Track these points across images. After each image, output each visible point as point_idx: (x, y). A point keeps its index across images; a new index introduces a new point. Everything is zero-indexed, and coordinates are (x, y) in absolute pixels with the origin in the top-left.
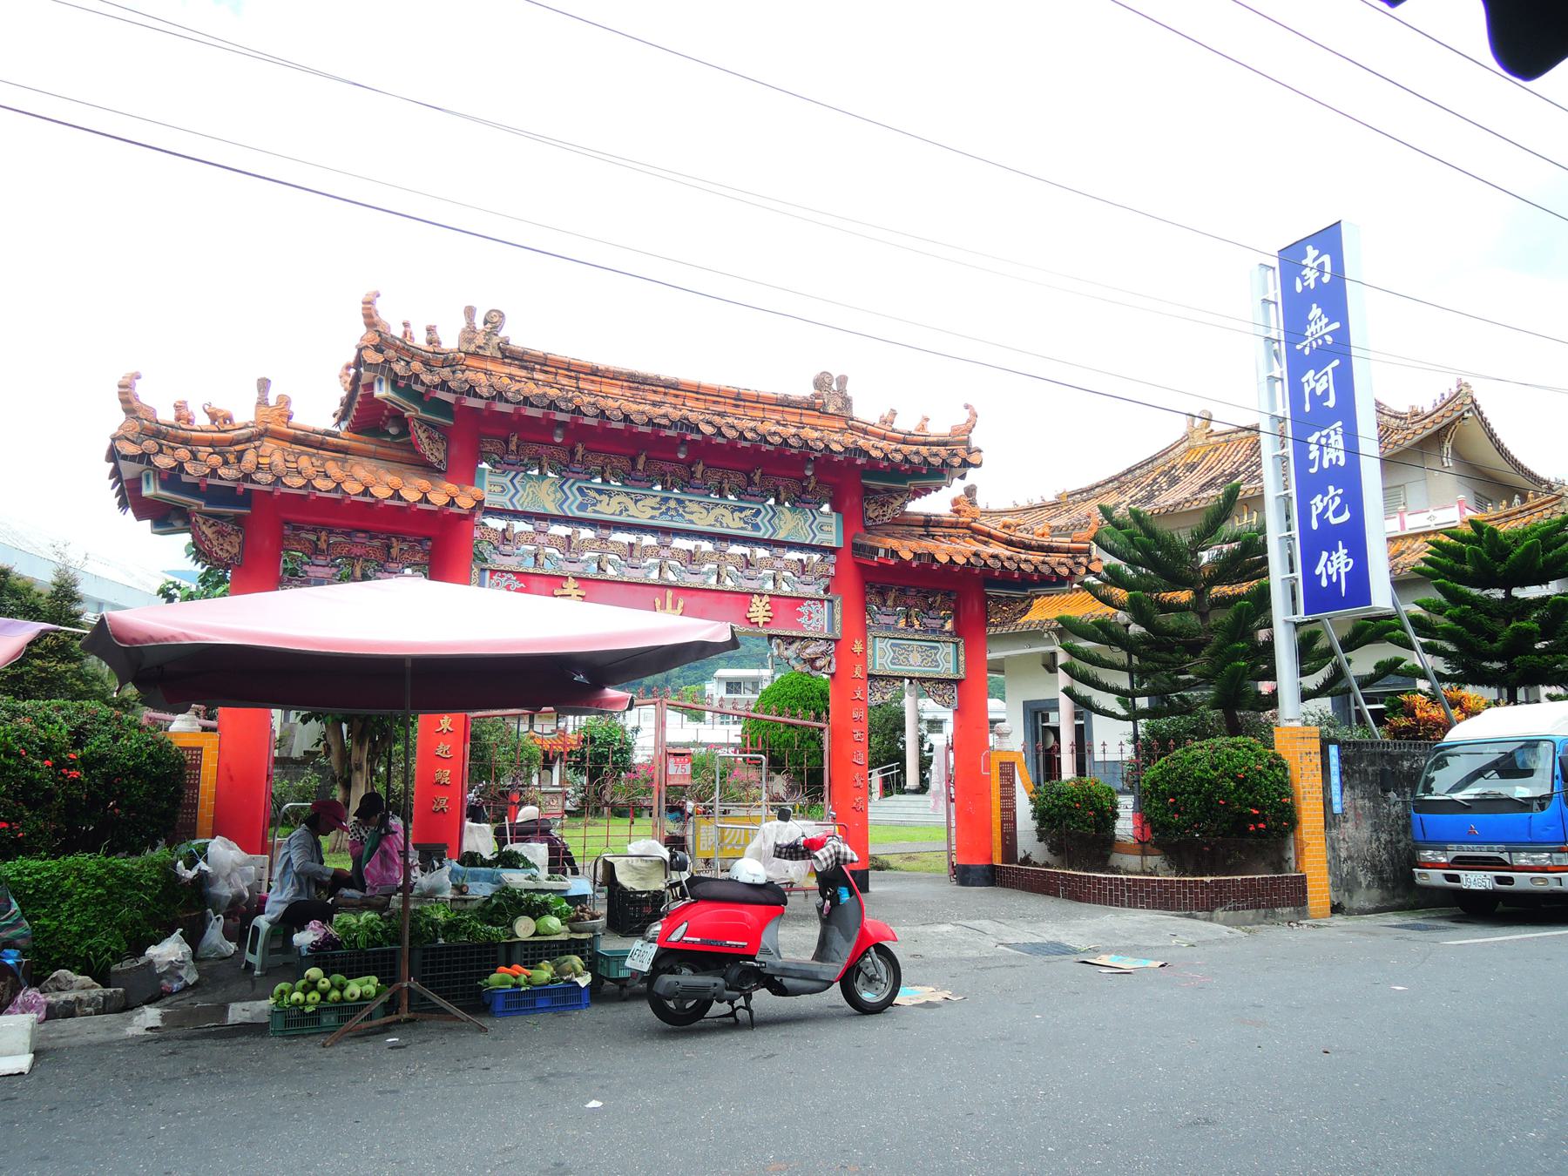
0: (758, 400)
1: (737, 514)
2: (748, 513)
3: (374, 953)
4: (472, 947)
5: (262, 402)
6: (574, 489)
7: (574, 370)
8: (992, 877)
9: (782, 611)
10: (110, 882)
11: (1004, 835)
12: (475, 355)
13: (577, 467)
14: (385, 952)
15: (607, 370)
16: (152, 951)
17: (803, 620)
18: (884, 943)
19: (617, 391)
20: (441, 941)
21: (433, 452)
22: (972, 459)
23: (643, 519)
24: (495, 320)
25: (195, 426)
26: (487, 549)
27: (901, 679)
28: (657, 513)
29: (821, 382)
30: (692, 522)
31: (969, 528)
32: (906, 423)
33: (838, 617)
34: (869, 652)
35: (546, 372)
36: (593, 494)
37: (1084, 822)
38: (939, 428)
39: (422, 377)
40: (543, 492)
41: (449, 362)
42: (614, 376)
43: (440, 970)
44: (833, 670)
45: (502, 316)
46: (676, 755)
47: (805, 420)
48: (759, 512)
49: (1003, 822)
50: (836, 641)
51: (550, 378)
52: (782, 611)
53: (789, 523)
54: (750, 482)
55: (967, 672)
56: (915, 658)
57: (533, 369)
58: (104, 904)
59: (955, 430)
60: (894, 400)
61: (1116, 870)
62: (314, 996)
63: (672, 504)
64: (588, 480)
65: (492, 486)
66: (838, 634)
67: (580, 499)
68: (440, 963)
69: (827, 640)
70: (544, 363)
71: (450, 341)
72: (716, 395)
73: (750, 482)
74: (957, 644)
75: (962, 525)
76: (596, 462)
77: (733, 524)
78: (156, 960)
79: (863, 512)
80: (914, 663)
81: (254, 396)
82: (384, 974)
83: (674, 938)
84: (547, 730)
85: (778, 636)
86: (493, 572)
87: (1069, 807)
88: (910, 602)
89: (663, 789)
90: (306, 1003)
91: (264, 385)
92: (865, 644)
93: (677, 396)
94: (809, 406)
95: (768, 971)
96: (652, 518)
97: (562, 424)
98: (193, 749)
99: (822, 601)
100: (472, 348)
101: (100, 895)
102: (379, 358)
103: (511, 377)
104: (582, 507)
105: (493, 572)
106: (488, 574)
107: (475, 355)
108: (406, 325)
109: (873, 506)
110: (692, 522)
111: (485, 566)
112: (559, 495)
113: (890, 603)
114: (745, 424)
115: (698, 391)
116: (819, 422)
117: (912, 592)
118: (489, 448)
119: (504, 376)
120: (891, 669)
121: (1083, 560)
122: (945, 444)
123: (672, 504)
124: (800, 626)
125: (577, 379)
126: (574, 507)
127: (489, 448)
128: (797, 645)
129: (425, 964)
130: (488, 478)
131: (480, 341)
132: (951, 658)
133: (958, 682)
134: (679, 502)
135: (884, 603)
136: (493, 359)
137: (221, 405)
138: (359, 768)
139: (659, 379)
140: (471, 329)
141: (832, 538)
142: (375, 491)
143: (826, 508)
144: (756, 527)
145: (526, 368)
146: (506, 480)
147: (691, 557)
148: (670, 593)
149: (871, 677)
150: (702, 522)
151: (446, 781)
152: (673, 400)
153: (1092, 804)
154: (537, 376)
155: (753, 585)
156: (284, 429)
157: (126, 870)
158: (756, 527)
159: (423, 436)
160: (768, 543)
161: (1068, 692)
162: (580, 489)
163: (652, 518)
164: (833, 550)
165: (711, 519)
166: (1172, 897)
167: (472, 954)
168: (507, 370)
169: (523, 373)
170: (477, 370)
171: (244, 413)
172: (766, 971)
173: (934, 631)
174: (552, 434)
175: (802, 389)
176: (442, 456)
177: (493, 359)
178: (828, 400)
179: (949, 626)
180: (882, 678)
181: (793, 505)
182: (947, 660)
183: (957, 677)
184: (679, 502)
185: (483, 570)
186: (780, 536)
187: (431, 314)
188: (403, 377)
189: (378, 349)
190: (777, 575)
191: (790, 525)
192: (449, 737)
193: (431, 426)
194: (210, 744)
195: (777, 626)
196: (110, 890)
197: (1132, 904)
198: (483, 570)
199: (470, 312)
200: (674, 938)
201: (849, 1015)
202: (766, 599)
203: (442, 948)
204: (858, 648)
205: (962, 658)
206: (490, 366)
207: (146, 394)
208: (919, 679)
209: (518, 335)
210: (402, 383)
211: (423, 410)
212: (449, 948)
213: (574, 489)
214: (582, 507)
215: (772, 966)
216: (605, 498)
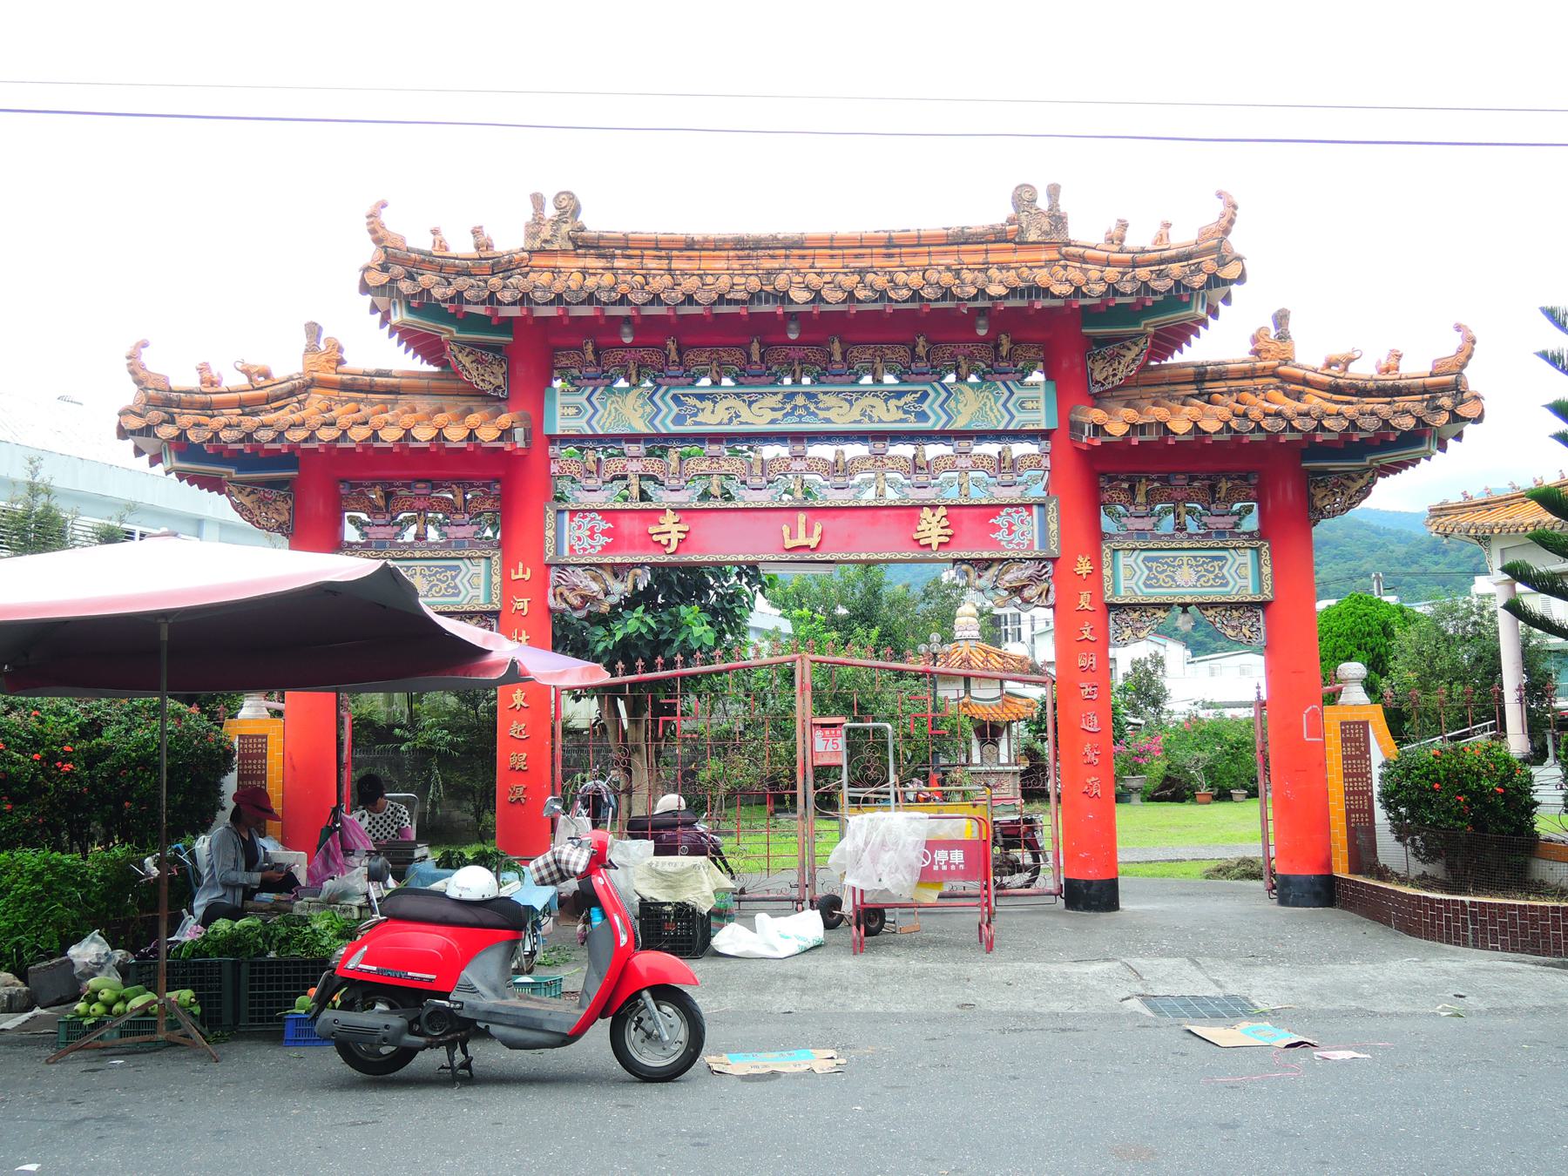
0: (920, 242)
1: (893, 403)
2: (909, 398)
3: (200, 964)
4: (306, 962)
5: (311, 349)
6: (668, 398)
7: (663, 248)
8: (1325, 892)
9: (967, 525)
10: (48, 877)
11: (1352, 832)
12: (541, 251)
13: (674, 370)
14: (212, 963)
15: (706, 240)
16: (73, 951)
17: (998, 536)
18: (687, 989)
19: (723, 264)
20: (272, 954)
21: (491, 378)
22: (1230, 272)
23: (761, 426)
24: (569, 207)
25: (223, 388)
26: (564, 486)
27: (1167, 607)
28: (779, 415)
29: (1023, 198)
30: (828, 421)
31: (1275, 375)
32: (1140, 238)
33: (1054, 527)
34: (1107, 572)
35: (629, 257)
36: (692, 401)
37: (1448, 812)
38: (1183, 236)
39: (1152, 284)
40: (628, 408)
41: (505, 267)
42: (716, 246)
43: (270, 988)
44: (1051, 600)
45: (571, 196)
46: (823, 726)
47: (992, 258)
48: (925, 395)
49: (1349, 812)
50: (1054, 560)
51: (635, 263)
52: (967, 525)
53: (971, 403)
54: (914, 357)
55: (1275, 590)
56: (1186, 575)
57: (613, 256)
58: (42, 900)
59: (1204, 234)
60: (1122, 208)
61: (1540, 889)
62: (98, 1008)
63: (800, 400)
64: (855, 383)
65: (567, 409)
66: (1054, 549)
67: (676, 409)
68: (270, 980)
69: (1040, 560)
70: (626, 245)
71: (509, 240)
72: (861, 245)
73: (914, 357)
74: (1258, 550)
75: (1270, 370)
76: (862, 355)
77: (888, 416)
78: (75, 960)
79: (1086, 376)
80: (1186, 579)
81: (302, 341)
82: (201, 989)
83: (351, 965)
84: (952, 695)
85: (963, 561)
86: (573, 513)
87: (1422, 789)
88: (1177, 495)
89: (809, 770)
90: (87, 1015)
91: (314, 330)
92: (1097, 561)
93: (803, 257)
94: (998, 237)
95: (465, 1014)
96: (773, 422)
97: (627, 320)
98: (257, 737)
99: (1028, 506)
100: (537, 244)
101: (37, 892)
102: (384, 278)
103: (584, 272)
104: (679, 420)
105: (573, 513)
106: (567, 515)
107: (541, 251)
108: (435, 232)
109: (1099, 365)
110: (828, 421)
111: (562, 506)
112: (649, 408)
113: (1140, 499)
114: (908, 280)
115: (832, 245)
116: (1015, 257)
117: (1180, 480)
118: (565, 362)
119: (573, 274)
120: (1143, 594)
121: (1446, 401)
122: (1188, 257)
123: (800, 400)
124: (996, 544)
125: (670, 258)
126: (668, 422)
127: (565, 362)
128: (994, 570)
129: (253, 980)
130: (559, 399)
131: (546, 233)
132: (1249, 571)
133: (1264, 605)
134: (810, 396)
135: (1132, 501)
136: (564, 252)
137: (257, 360)
138: (637, 749)
139: (775, 238)
140: (538, 221)
141: (1041, 415)
142: (1204, 425)
143: (1037, 377)
144: (922, 416)
145: (604, 256)
146: (581, 399)
147: (838, 469)
148: (802, 517)
149: (1111, 607)
150: (842, 417)
151: (522, 765)
152: (796, 263)
153: (1462, 783)
154: (618, 263)
155: (927, 495)
156: (332, 376)
157: (68, 866)
158: (922, 416)
159: (466, 361)
160: (944, 436)
161: (1515, 608)
162: (675, 398)
163: (773, 422)
164: (1045, 435)
165: (856, 413)
166: (1545, 935)
167: (305, 971)
168: (581, 263)
169: (601, 263)
170: (542, 269)
171: (288, 364)
172: (463, 1014)
173: (1221, 533)
174: (618, 334)
175: (993, 212)
176: (500, 381)
177: (564, 252)
178: (1035, 225)
179: (1251, 523)
180: (1133, 607)
181: (983, 377)
182: (1243, 574)
183: (489, 607)
184: (810, 396)
185: (561, 512)
186: (960, 424)
187: (476, 209)
188: (414, 296)
189: (384, 268)
190: (962, 477)
191: (973, 407)
192: (525, 713)
193: (464, 345)
194: (275, 733)
195: (960, 547)
196: (49, 887)
197: (1480, 943)
198: (561, 512)
199: (538, 201)
200: (351, 965)
201: (617, 1081)
202: (942, 511)
203: (272, 962)
204: (1084, 567)
205: (1267, 570)
206: (560, 262)
207: (154, 362)
208: (1199, 605)
209: (597, 220)
210: (415, 303)
211: (461, 330)
212: (279, 963)
213: (668, 398)
214: (679, 420)
215: (473, 1009)
216: (708, 404)
